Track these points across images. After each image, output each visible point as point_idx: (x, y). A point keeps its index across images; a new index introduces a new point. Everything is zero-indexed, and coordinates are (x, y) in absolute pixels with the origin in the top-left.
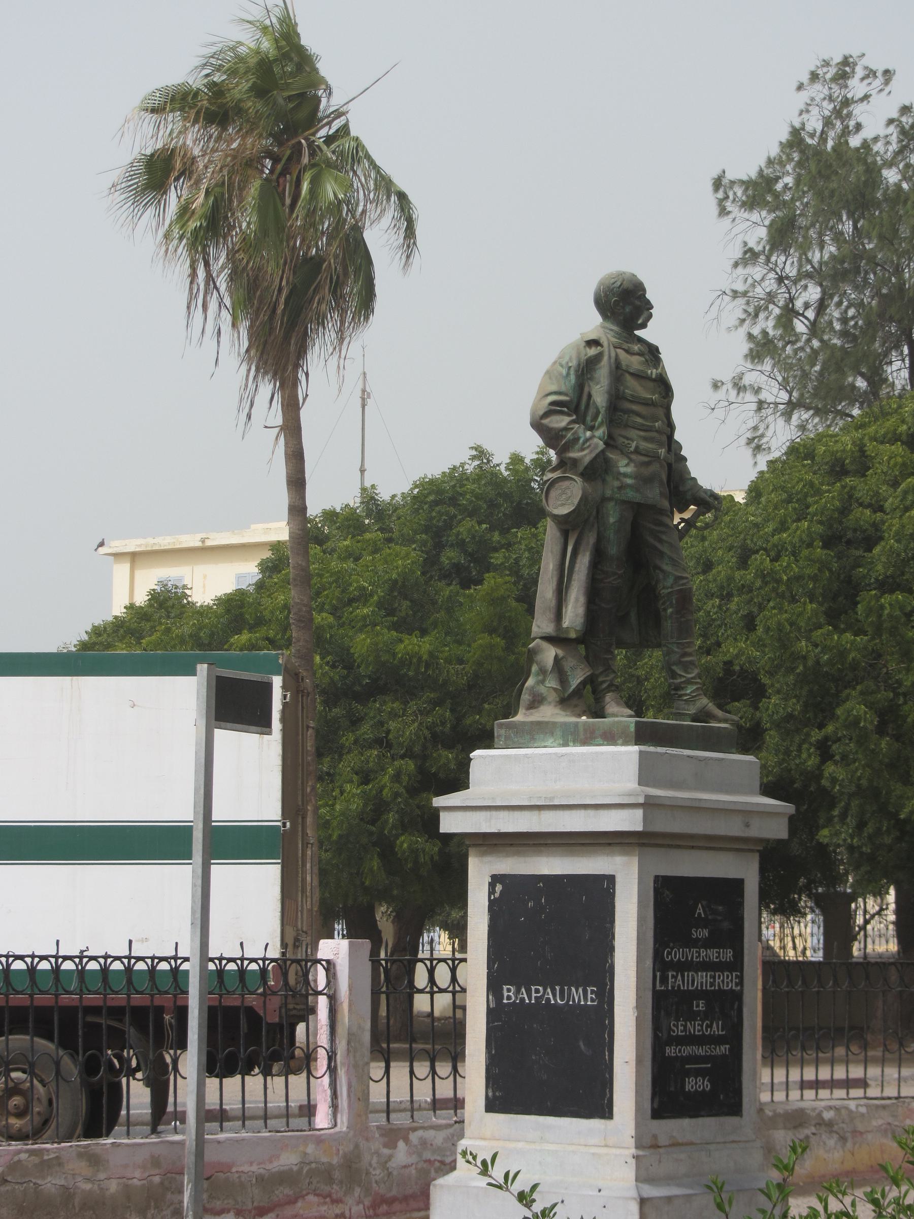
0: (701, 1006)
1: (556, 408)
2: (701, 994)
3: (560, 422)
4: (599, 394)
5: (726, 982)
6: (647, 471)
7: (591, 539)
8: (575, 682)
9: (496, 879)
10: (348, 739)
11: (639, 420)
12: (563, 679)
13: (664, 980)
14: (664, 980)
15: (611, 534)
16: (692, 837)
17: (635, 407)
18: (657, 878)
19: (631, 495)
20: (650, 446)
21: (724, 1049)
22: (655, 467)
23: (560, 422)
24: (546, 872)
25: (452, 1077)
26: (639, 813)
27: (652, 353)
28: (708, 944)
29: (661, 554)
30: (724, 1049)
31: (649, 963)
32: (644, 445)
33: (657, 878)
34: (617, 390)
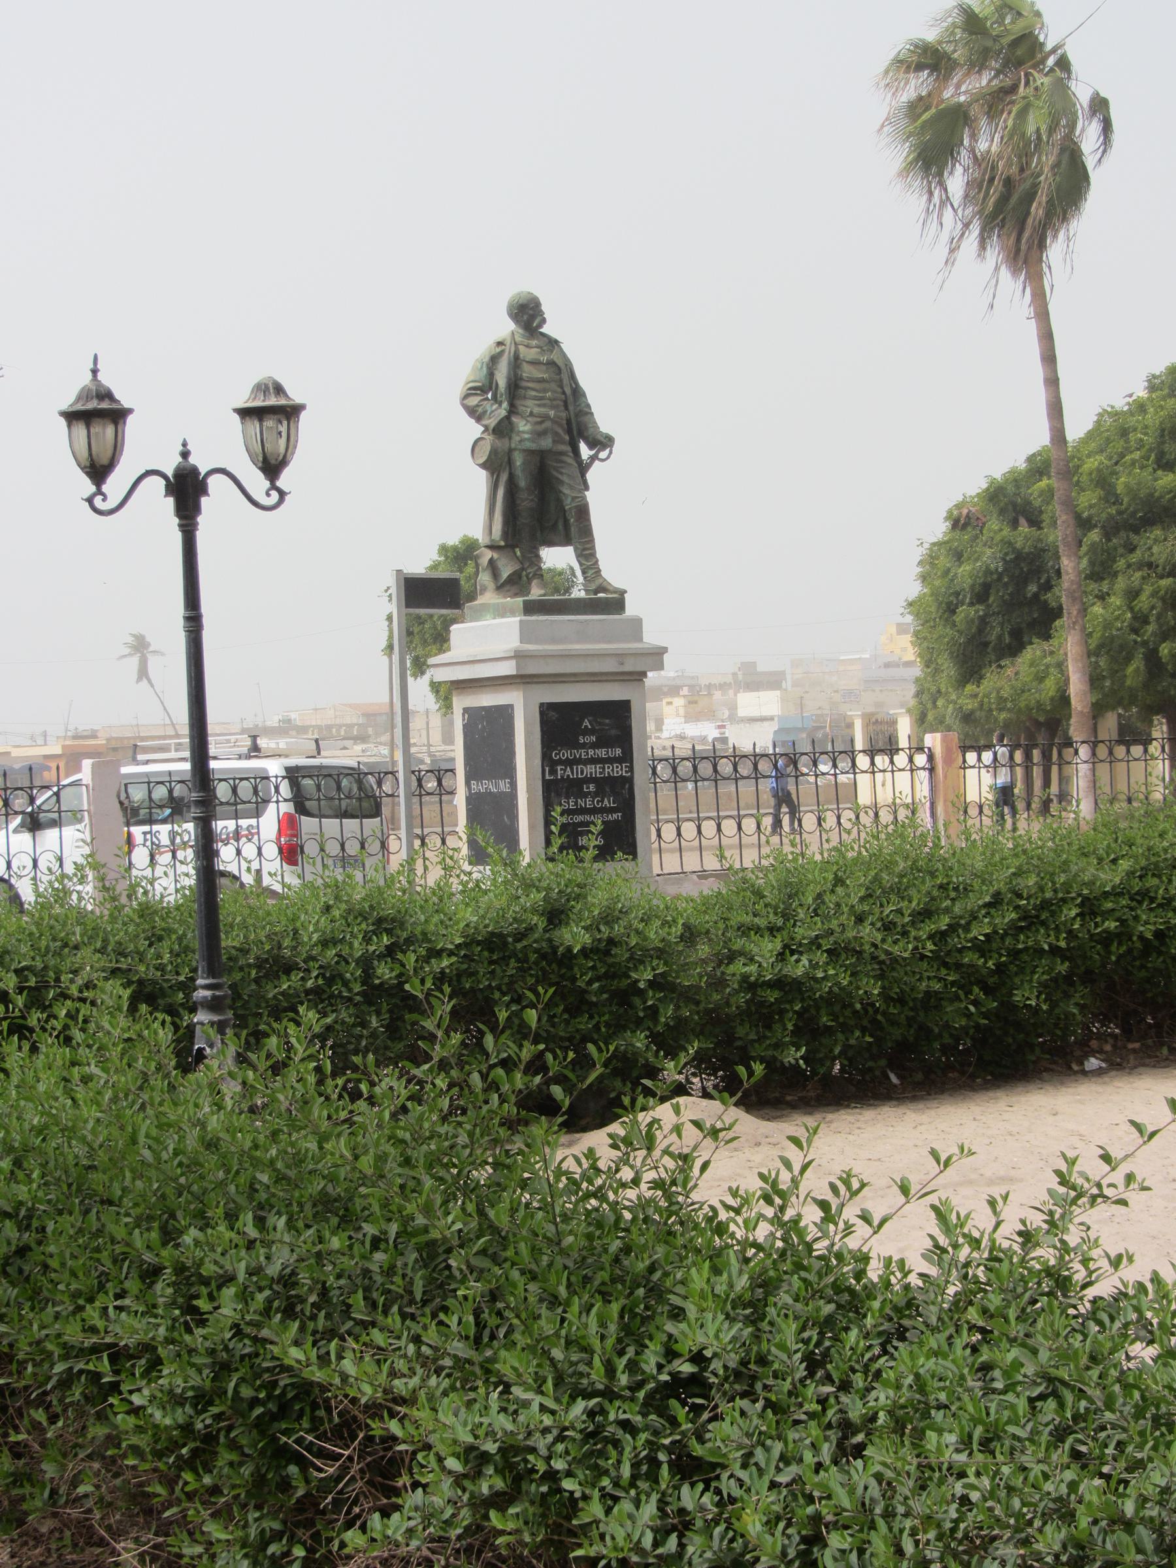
0: (592, 787)
1: (472, 391)
2: (592, 780)
3: (473, 401)
4: (501, 379)
5: (618, 771)
6: (540, 428)
7: (504, 477)
8: (505, 575)
9: (466, 710)
10: (1121, 564)
11: (533, 393)
12: (495, 574)
13: (553, 772)
14: (553, 772)
15: (519, 473)
16: (574, 675)
17: (530, 385)
18: (542, 705)
19: (528, 445)
20: (543, 410)
21: (616, 816)
22: (548, 424)
23: (473, 401)
24: (485, 704)
25: (12, 852)
26: (513, 663)
27: (553, 343)
28: (594, 746)
29: (562, 482)
30: (616, 816)
31: (538, 762)
32: (536, 410)
33: (542, 705)
34: (516, 375)
